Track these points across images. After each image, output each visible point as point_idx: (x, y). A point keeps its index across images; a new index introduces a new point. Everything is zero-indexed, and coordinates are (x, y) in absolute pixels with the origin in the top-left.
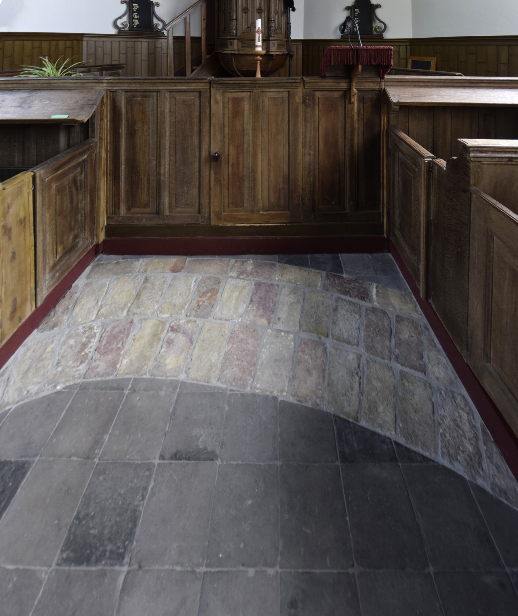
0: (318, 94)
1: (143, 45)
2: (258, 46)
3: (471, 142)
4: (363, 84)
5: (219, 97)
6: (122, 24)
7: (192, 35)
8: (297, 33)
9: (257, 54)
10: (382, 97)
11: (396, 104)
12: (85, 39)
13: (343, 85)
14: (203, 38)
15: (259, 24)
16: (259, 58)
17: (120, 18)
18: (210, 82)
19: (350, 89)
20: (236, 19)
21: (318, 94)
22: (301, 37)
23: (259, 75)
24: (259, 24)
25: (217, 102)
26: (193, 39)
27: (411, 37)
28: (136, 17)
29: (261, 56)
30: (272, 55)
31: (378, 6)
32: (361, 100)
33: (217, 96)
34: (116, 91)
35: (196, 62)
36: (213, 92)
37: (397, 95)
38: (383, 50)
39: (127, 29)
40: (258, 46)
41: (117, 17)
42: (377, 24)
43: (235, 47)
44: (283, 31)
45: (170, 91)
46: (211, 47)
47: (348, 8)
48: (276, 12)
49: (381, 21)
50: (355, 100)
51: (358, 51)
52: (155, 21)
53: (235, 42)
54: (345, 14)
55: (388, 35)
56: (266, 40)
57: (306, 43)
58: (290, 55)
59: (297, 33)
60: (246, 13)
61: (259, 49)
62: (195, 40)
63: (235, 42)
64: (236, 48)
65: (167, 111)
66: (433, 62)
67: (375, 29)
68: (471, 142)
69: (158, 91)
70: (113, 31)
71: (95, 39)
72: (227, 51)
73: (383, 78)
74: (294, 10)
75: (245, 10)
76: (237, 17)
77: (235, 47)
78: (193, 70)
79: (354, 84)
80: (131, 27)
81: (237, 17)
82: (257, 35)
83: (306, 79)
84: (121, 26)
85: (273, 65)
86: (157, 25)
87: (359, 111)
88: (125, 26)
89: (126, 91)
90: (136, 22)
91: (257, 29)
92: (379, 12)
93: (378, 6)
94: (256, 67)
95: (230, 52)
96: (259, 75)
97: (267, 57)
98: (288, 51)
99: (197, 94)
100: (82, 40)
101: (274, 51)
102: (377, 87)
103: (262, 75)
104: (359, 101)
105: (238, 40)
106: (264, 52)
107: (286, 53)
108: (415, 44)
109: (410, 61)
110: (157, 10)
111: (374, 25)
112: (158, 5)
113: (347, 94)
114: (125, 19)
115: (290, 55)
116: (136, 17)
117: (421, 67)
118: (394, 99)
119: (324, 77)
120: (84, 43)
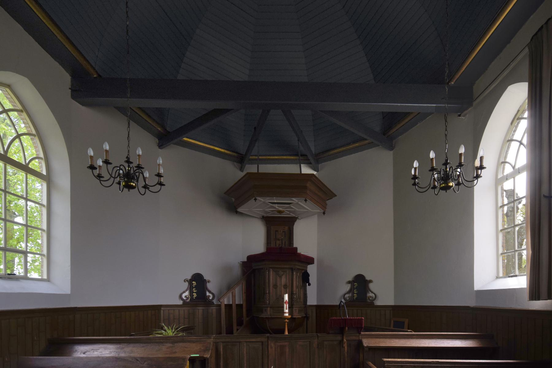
0: (326, 343)
1: (200, 310)
2: (286, 313)
3: (385, 360)
4: (349, 337)
5: (272, 345)
6: (186, 296)
7: (237, 303)
8: (312, 300)
9: (286, 318)
10: (360, 343)
11: (366, 347)
12: (162, 308)
13: (339, 338)
14: (244, 306)
15: (286, 297)
16: (287, 320)
17: (184, 292)
18: (268, 337)
19: (343, 340)
20: (269, 293)
21: (326, 343)
22: (315, 303)
23: (287, 333)
24: (286, 297)
25: (272, 348)
26: (237, 305)
27: (393, 304)
28: (195, 291)
29: (288, 319)
30: (295, 318)
31: (371, 281)
32: (349, 346)
33: (272, 344)
34: (218, 342)
35: (240, 324)
36: (269, 342)
37: (366, 343)
38: (359, 319)
39: (188, 300)
40: (286, 313)
41: (182, 292)
42: (370, 294)
43: (268, 313)
44: (302, 300)
45: (246, 342)
46: (249, 311)
47: (349, 282)
48: (297, 287)
49: (372, 292)
50: (345, 345)
51: (346, 320)
52: (208, 294)
53: (269, 309)
54: (348, 287)
55: (378, 303)
56: (290, 308)
57: (319, 308)
58: (307, 318)
59: (312, 300)
60: (276, 288)
61: (287, 315)
62: (239, 306)
63: (269, 309)
64: (269, 313)
65: (245, 353)
66: (406, 321)
67: (369, 298)
68: (385, 360)
69: (240, 342)
70: (181, 303)
71: (168, 308)
72: (263, 315)
73: (360, 334)
74: (309, 285)
75: (275, 286)
76: (269, 291)
77: (268, 313)
78: (237, 330)
79: (344, 337)
80: (192, 299)
81: (269, 291)
82: (285, 305)
83: (319, 334)
84: (185, 299)
85: (295, 324)
86: (209, 296)
87: (348, 352)
88: (188, 298)
89: (223, 342)
90: (195, 295)
91: (285, 301)
92: (371, 286)
93: (371, 281)
94: (285, 327)
95: (265, 317)
96: (287, 333)
97: (292, 319)
98: (306, 314)
99: (261, 343)
100: (161, 309)
101: (297, 315)
102: (357, 338)
103: (288, 333)
104: (347, 346)
105: (271, 307)
106: (290, 316)
107: (305, 316)
108: (396, 309)
109: (392, 322)
110: (209, 286)
111: (368, 295)
112: (209, 282)
113: (341, 342)
114: (187, 293)
115: (307, 318)
116: (195, 291)
117: (399, 326)
118: (365, 345)
119: (329, 333)
120: (162, 311)
